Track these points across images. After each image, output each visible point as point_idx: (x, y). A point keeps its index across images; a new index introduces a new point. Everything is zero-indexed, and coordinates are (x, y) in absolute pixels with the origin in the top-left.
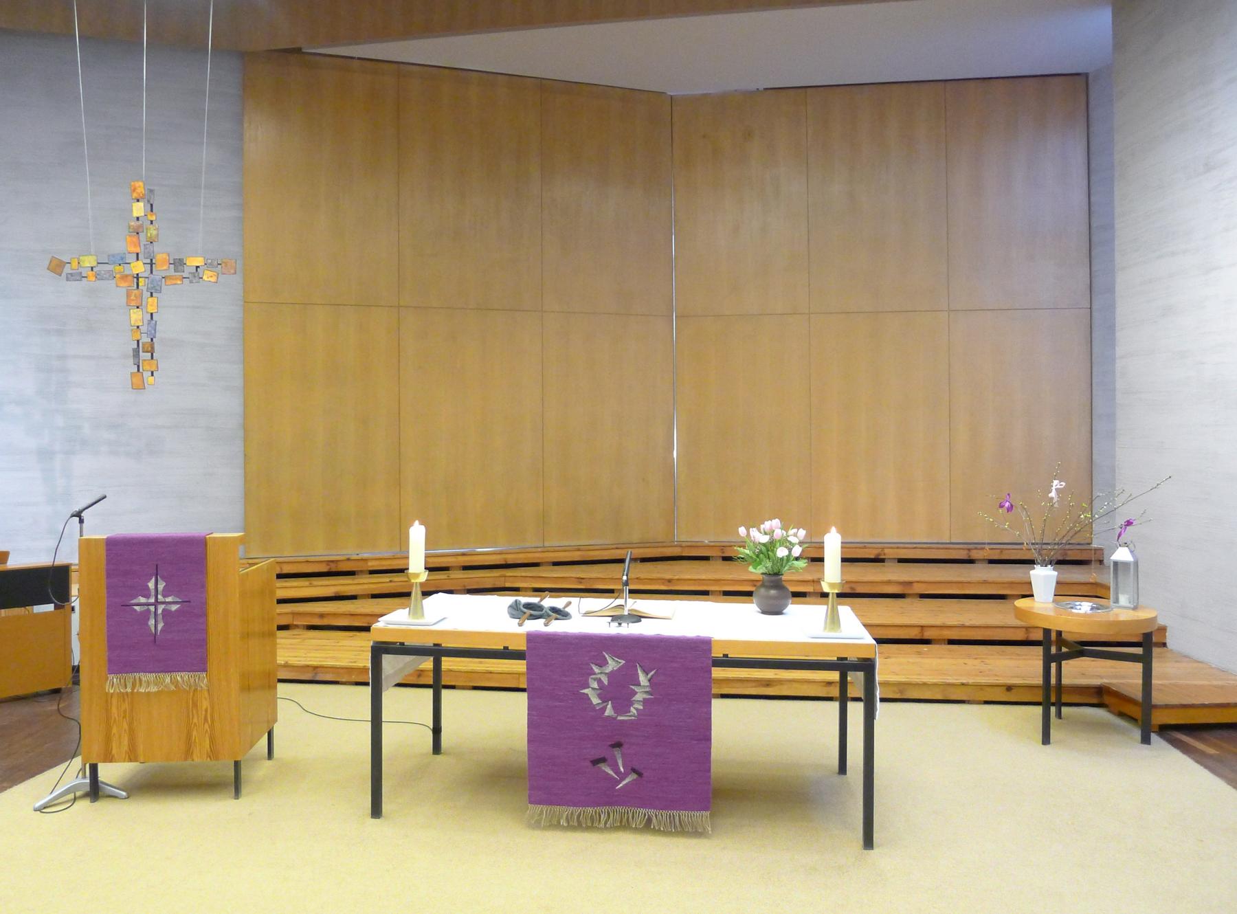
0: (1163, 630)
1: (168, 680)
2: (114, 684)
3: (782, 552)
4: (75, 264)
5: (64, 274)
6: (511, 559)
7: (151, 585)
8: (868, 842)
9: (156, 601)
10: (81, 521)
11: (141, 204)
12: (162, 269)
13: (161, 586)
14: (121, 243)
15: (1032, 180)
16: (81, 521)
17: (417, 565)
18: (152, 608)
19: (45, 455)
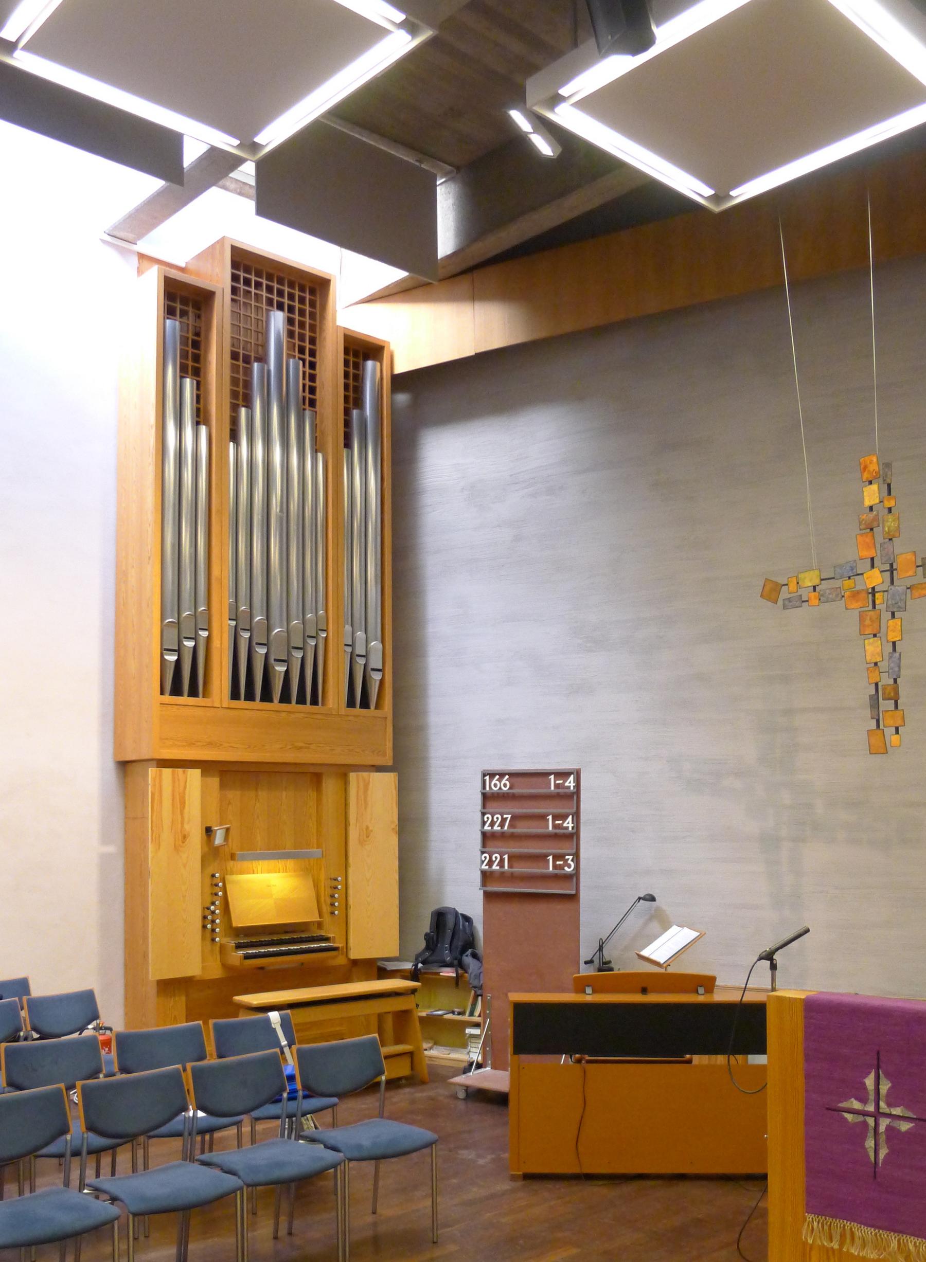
1: (894, 1244)
2: (814, 1230)
4: (793, 586)
5: (780, 602)
7: (869, 1082)
10: (773, 967)
11: (875, 487)
12: (907, 575)
13: (885, 1087)
14: (853, 549)
16: (773, 967)
18: (871, 1121)
19: (769, 842)
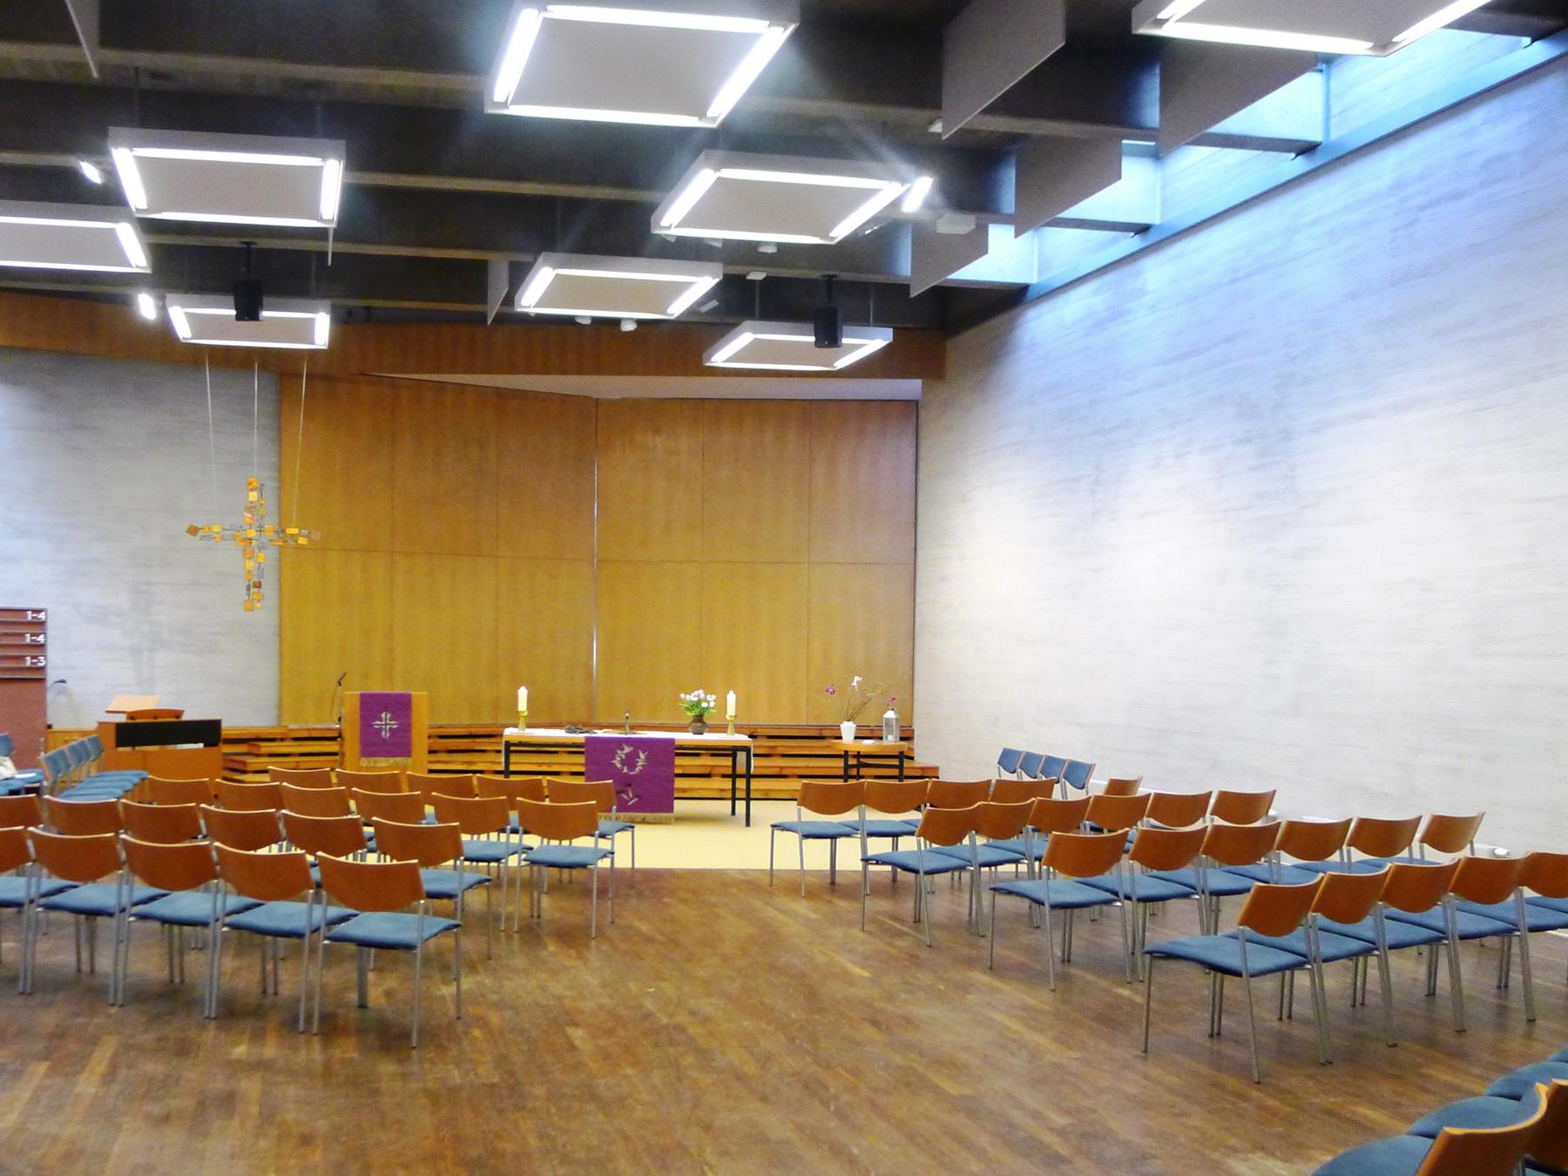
0: (936, 769)
3: (704, 705)
6: (474, 731)
8: (748, 824)
9: (386, 723)
15: (884, 456)
17: (522, 705)
19: (135, 651)
